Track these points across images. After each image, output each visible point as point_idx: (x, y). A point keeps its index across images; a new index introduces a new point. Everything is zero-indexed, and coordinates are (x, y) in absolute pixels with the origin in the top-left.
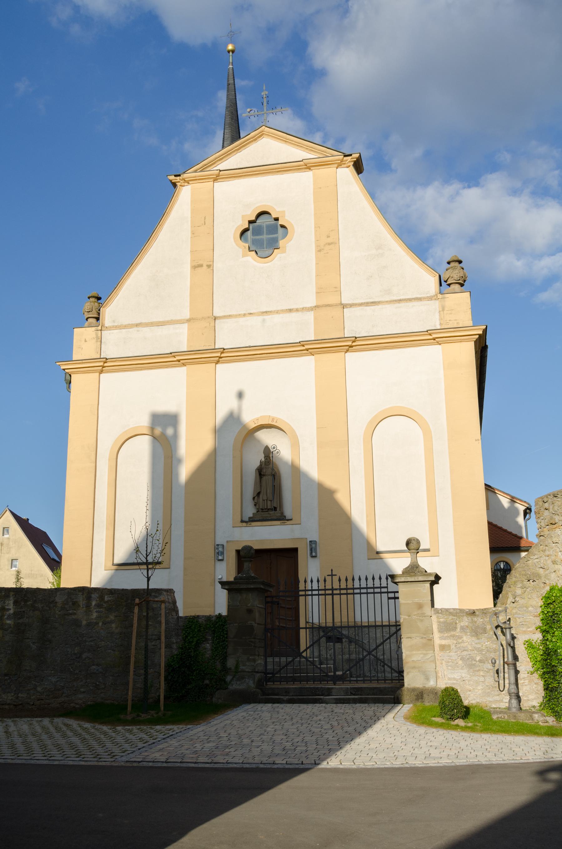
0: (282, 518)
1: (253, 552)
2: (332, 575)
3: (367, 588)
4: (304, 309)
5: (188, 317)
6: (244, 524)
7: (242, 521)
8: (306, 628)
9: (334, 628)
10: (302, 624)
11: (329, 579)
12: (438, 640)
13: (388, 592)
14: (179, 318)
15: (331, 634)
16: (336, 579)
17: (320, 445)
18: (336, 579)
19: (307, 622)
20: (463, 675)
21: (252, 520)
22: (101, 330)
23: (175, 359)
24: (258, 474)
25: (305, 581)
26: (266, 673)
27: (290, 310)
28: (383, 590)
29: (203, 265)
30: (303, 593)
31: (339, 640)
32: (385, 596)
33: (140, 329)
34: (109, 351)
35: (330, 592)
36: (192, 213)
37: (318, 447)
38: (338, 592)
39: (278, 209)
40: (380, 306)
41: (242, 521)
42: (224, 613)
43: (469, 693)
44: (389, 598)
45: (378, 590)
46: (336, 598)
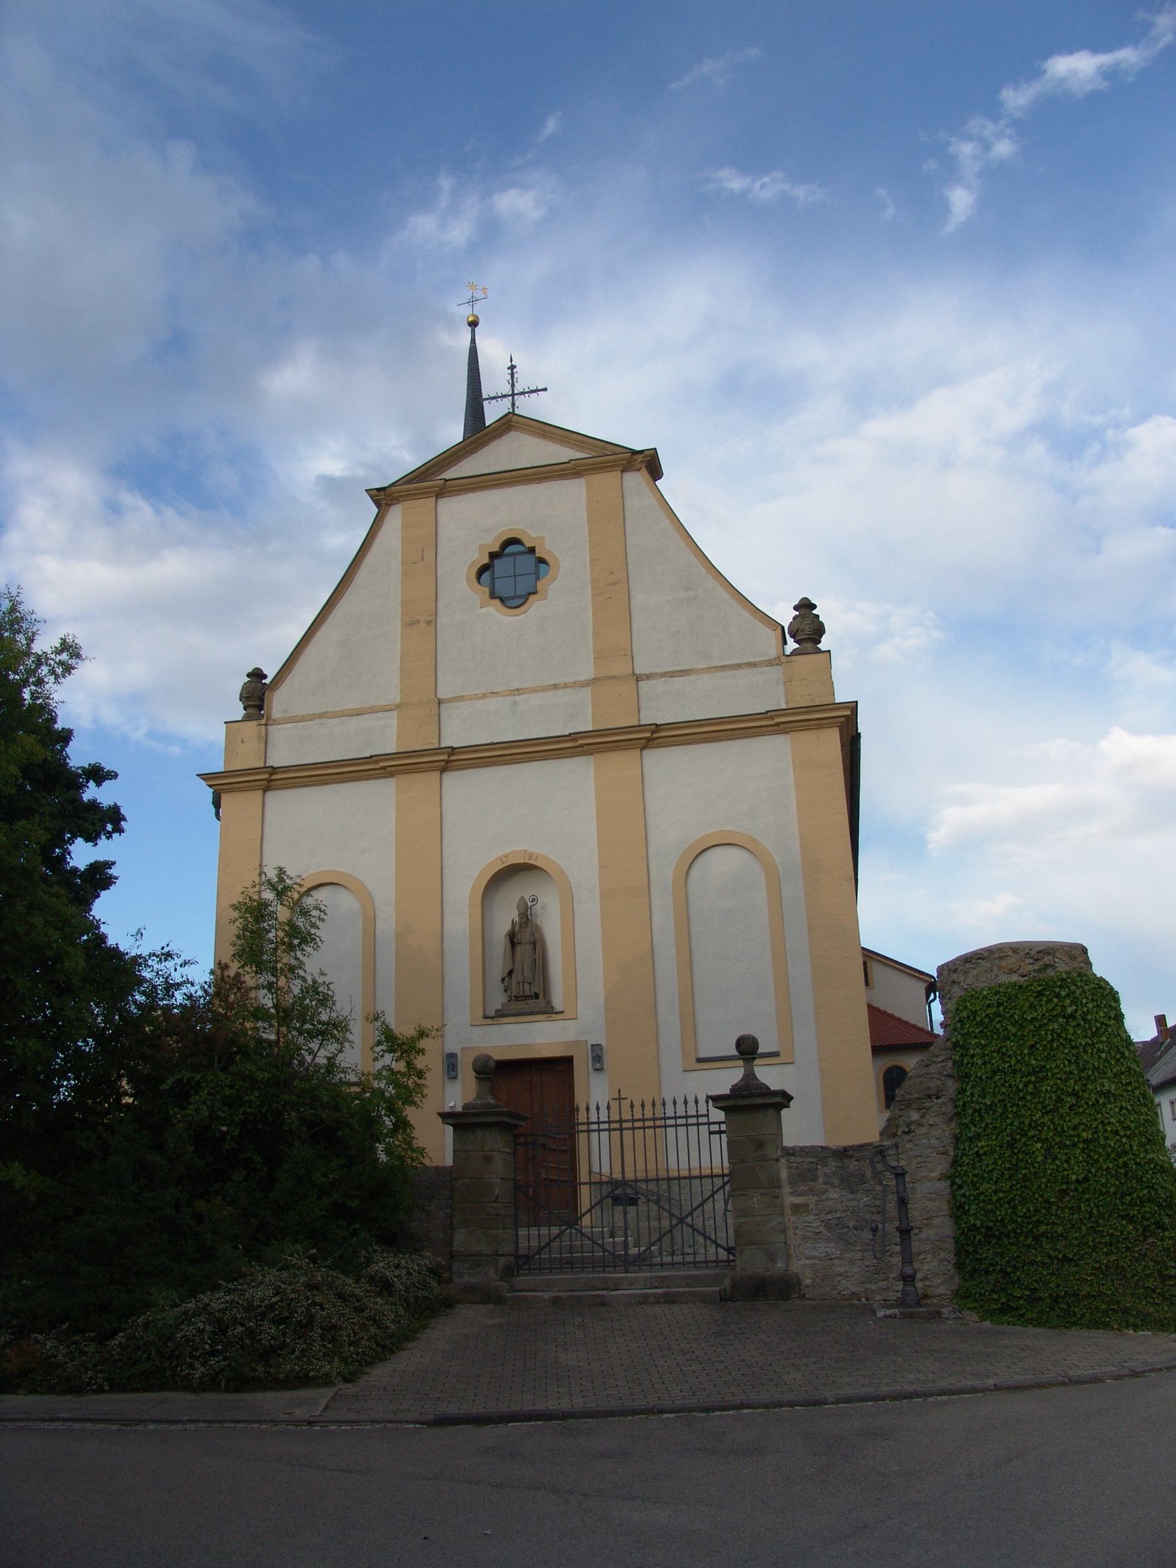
0: (549, 1011)
1: (492, 1064)
2: (620, 1099)
3: (686, 1117)
4: (576, 685)
5: (398, 701)
6: (489, 1021)
7: (486, 1017)
8: (590, 1183)
9: (624, 1183)
10: (583, 1176)
11: (615, 1105)
12: (790, 1200)
13: (709, 1124)
14: (383, 703)
15: (621, 1194)
16: (626, 1105)
17: (605, 895)
18: (626, 1105)
19: (590, 1172)
20: (829, 1251)
21: (501, 1014)
22: (266, 725)
23: (771, 722)
24: (509, 945)
25: (588, 1109)
26: (517, 1256)
27: (555, 687)
28: (702, 1120)
29: (421, 619)
30: (584, 1127)
31: (633, 1201)
32: (704, 1130)
33: (325, 721)
34: (279, 757)
35: (617, 1126)
36: (403, 544)
37: (601, 896)
38: (629, 1125)
39: (533, 535)
40: (693, 677)
41: (486, 1017)
42: (449, 1162)
43: (839, 1278)
44: (711, 1133)
45: (694, 1120)
46: (628, 1134)
